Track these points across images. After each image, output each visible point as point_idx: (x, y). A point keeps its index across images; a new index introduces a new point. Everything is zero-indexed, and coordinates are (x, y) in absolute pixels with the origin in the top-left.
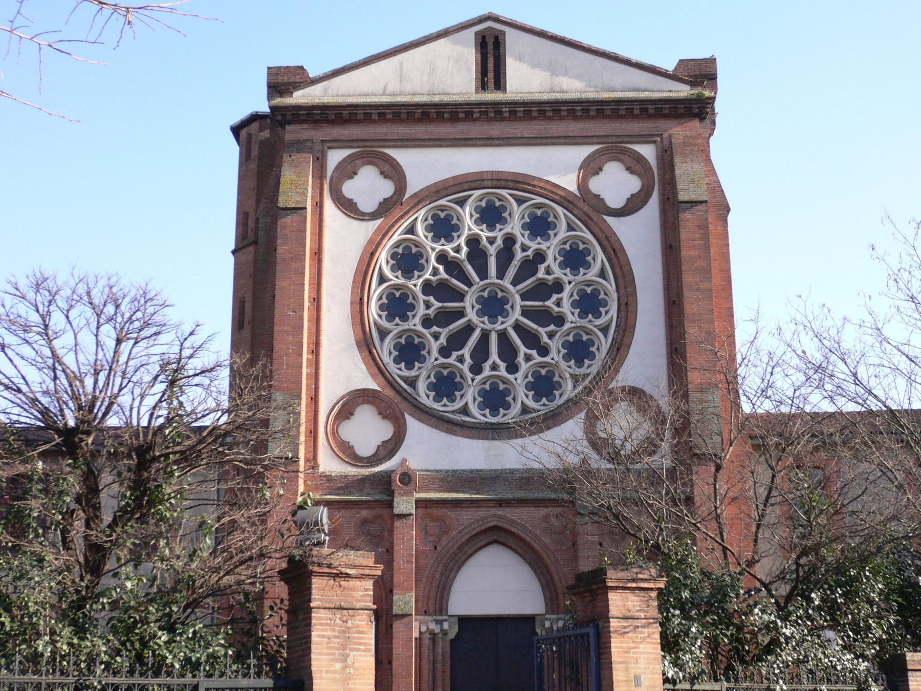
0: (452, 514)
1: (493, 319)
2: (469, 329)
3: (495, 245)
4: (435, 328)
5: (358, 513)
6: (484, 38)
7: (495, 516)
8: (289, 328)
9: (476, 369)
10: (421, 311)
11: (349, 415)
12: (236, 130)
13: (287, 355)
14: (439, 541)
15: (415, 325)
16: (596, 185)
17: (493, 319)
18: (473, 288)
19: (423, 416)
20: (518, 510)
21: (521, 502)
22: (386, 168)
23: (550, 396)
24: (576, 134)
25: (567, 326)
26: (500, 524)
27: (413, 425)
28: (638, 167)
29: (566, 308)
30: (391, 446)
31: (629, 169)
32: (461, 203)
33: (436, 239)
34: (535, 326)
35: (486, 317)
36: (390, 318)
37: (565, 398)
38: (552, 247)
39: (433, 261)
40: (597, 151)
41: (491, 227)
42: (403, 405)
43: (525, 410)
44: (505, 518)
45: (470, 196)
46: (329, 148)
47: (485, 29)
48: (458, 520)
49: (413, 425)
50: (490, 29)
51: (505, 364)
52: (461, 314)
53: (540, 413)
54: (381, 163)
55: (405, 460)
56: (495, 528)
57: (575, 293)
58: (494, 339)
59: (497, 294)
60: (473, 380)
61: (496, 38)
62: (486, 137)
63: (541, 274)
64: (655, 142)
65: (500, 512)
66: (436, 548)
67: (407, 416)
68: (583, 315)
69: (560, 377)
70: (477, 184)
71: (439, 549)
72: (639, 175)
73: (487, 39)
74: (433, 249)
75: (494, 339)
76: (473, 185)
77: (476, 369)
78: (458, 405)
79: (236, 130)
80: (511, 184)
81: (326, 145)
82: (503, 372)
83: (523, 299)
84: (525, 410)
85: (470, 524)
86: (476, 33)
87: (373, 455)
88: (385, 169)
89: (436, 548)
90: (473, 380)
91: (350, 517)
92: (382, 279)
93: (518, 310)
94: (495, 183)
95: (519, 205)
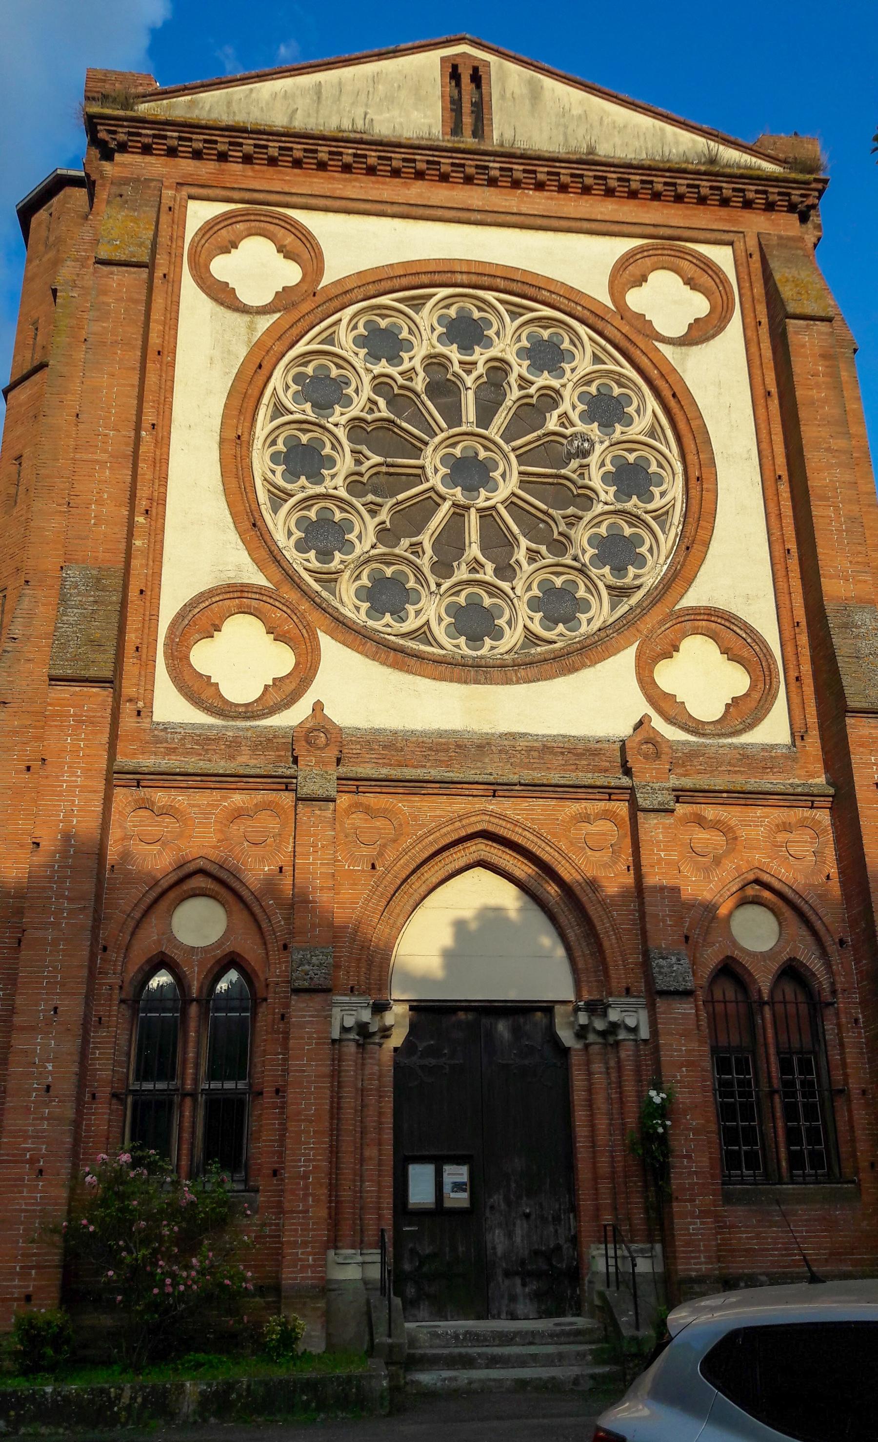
0: (403, 805)
1: (471, 489)
2: (432, 500)
3: (475, 374)
4: (370, 497)
5: (224, 798)
6: (455, 67)
7: (484, 812)
8: (104, 457)
9: (443, 568)
10: (345, 464)
11: (211, 629)
12: (217, 684)
13: (100, 502)
14: (381, 854)
15: (336, 488)
16: (635, 299)
17: (471, 489)
18: (437, 440)
19: (350, 637)
20: (524, 804)
21: (536, 789)
22: (289, 240)
23: (569, 620)
24: (607, 218)
25: (599, 508)
26: (492, 828)
27: (329, 646)
28: (705, 279)
29: (596, 480)
30: (290, 687)
31: (689, 282)
32: (417, 304)
33: (374, 357)
34: (515, 529)
35: (459, 488)
36: (292, 474)
37: (596, 625)
38: (571, 384)
39: (367, 391)
40: (641, 250)
41: (467, 348)
42: (314, 616)
43: (532, 638)
44: (502, 817)
45: (431, 296)
46: (191, 197)
47: (456, 55)
48: (415, 818)
49: (329, 646)
50: (464, 55)
51: (494, 566)
52: (419, 476)
53: (555, 645)
54: (280, 233)
55: (318, 706)
56: (485, 835)
57: (608, 461)
58: (473, 519)
59: (477, 454)
60: (439, 585)
61: (476, 69)
62: (460, 206)
63: (552, 423)
64: (731, 243)
65: (493, 806)
66: (373, 867)
67: (321, 634)
68: (623, 494)
69: (509, 623)
70: (444, 278)
71: (380, 869)
72: (707, 294)
73: (461, 70)
74: (368, 370)
75: (473, 519)
76: (437, 278)
77: (443, 568)
78: (412, 624)
79: (217, 684)
80: (501, 284)
81: (185, 191)
82: (488, 574)
83: (520, 464)
84: (532, 638)
85: (439, 827)
86: (443, 60)
87: (256, 701)
88: (286, 242)
89: (373, 867)
90: (439, 585)
91: (208, 805)
92: (279, 410)
93: (515, 478)
94: (474, 279)
95: (512, 320)
